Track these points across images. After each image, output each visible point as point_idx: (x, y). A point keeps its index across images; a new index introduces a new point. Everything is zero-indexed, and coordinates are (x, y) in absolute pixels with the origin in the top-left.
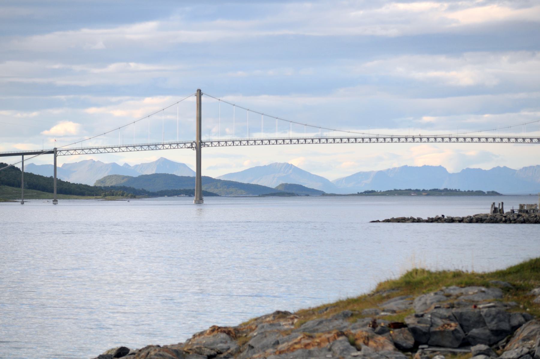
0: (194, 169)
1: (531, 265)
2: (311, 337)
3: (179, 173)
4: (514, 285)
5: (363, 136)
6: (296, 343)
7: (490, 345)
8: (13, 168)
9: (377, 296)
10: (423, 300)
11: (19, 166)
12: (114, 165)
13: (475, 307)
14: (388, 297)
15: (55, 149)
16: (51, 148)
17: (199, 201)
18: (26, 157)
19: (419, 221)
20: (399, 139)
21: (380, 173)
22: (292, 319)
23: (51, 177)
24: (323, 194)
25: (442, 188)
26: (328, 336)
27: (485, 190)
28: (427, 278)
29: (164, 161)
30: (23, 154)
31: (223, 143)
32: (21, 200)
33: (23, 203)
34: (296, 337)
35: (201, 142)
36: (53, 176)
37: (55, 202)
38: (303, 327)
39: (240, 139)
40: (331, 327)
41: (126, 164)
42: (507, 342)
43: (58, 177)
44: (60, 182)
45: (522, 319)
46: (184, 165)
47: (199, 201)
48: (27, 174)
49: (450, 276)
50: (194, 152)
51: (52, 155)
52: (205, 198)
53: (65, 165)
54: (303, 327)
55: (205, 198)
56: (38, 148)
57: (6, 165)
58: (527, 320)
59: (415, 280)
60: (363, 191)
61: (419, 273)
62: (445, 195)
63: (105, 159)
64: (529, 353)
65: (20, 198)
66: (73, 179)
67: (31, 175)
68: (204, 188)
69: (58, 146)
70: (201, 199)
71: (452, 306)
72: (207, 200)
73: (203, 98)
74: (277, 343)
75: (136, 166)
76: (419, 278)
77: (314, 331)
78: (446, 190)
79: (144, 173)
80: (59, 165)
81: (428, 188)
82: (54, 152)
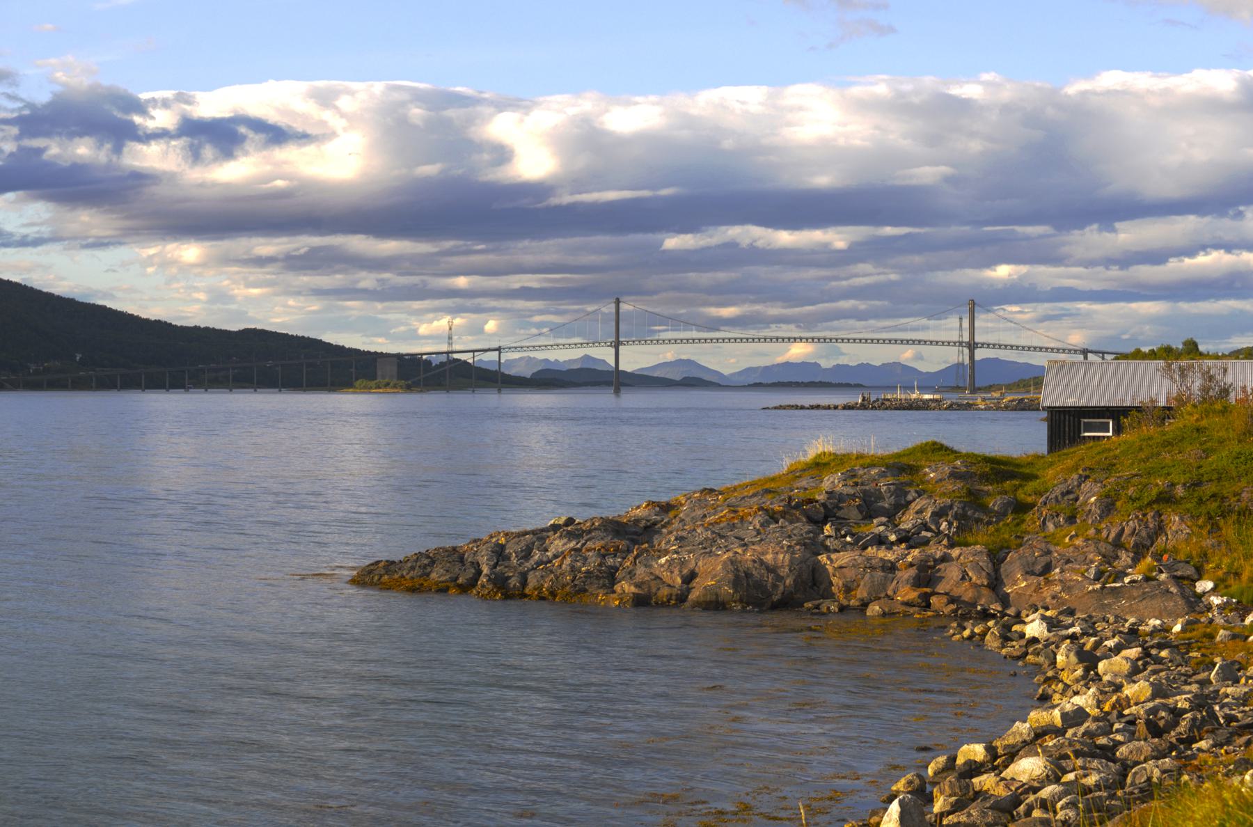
0: (613, 364)
1: (921, 448)
2: (735, 512)
3: (600, 368)
4: (909, 466)
5: (747, 336)
6: (722, 517)
7: (889, 518)
8: (465, 362)
9: (791, 476)
10: (832, 479)
11: (471, 361)
12: (546, 361)
13: (877, 485)
14: (800, 477)
15: (500, 347)
16: (496, 346)
17: (617, 392)
18: (476, 354)
19: (802, 408)
20: (783, 339)
21: (766, 368)
22: (717, 495)
23: (496, 371)
24: (719, 385)
25: (817, 380)
26: (750, 510)
27: (852, 383)
28: (834, 460)
29: (587, 358)
30: (474, 351)
31: (649, 342)
32: (980, 354)
33: (473, 391)
34: (722, 511)
35: (619, 341)
36: (497, 368)
37: (499, 391)
38: (726, 503)
39: (639, 339)
40: (752, 502)
41: (556, 360)
42: (903, 514)
43: (502, 370)
44: (503, 375)
45: (914, 495)
46: (604, 361)
47: (617, 392)
48: (477, 368)
49: (854, 458)
50: (612, 351)
51: (497, 352)
52: (622, 388)
53: (507, 361)
54: (726, 503)
55: (622, 388)
56: (486, 347)
57: (460, 360)
58: (919, 496)
59: (823, 461)
60: (752, 383)
61: (826, 456)
62: (820, 387)
63: (540, 355)
64: (922, 523)
65: (471, 387)
66: (512, 372)
67: (480, 369)
68: (621, 380)
69: (502, 344)
70: (619, 389)
71: (856, 484)
72: (623, 390)
73: (621, 305)
74: (705, 516)
75: (565, 361)
76: (826, 460)
77: (737, 506)
78: (820, 382)
79: (572, 367)
80: (502, 361)
81: (770, 382)
82: (499, 349)
